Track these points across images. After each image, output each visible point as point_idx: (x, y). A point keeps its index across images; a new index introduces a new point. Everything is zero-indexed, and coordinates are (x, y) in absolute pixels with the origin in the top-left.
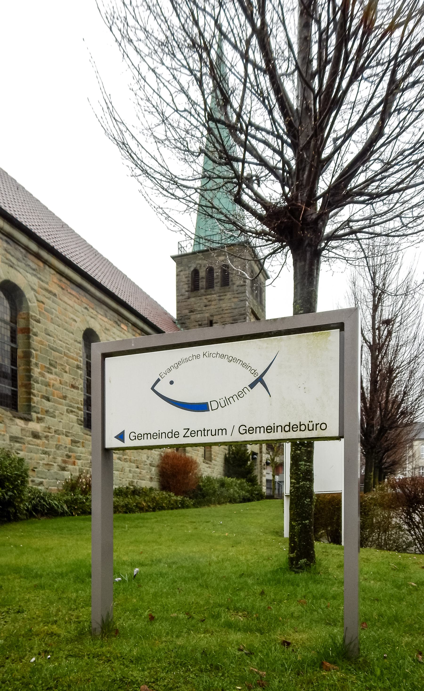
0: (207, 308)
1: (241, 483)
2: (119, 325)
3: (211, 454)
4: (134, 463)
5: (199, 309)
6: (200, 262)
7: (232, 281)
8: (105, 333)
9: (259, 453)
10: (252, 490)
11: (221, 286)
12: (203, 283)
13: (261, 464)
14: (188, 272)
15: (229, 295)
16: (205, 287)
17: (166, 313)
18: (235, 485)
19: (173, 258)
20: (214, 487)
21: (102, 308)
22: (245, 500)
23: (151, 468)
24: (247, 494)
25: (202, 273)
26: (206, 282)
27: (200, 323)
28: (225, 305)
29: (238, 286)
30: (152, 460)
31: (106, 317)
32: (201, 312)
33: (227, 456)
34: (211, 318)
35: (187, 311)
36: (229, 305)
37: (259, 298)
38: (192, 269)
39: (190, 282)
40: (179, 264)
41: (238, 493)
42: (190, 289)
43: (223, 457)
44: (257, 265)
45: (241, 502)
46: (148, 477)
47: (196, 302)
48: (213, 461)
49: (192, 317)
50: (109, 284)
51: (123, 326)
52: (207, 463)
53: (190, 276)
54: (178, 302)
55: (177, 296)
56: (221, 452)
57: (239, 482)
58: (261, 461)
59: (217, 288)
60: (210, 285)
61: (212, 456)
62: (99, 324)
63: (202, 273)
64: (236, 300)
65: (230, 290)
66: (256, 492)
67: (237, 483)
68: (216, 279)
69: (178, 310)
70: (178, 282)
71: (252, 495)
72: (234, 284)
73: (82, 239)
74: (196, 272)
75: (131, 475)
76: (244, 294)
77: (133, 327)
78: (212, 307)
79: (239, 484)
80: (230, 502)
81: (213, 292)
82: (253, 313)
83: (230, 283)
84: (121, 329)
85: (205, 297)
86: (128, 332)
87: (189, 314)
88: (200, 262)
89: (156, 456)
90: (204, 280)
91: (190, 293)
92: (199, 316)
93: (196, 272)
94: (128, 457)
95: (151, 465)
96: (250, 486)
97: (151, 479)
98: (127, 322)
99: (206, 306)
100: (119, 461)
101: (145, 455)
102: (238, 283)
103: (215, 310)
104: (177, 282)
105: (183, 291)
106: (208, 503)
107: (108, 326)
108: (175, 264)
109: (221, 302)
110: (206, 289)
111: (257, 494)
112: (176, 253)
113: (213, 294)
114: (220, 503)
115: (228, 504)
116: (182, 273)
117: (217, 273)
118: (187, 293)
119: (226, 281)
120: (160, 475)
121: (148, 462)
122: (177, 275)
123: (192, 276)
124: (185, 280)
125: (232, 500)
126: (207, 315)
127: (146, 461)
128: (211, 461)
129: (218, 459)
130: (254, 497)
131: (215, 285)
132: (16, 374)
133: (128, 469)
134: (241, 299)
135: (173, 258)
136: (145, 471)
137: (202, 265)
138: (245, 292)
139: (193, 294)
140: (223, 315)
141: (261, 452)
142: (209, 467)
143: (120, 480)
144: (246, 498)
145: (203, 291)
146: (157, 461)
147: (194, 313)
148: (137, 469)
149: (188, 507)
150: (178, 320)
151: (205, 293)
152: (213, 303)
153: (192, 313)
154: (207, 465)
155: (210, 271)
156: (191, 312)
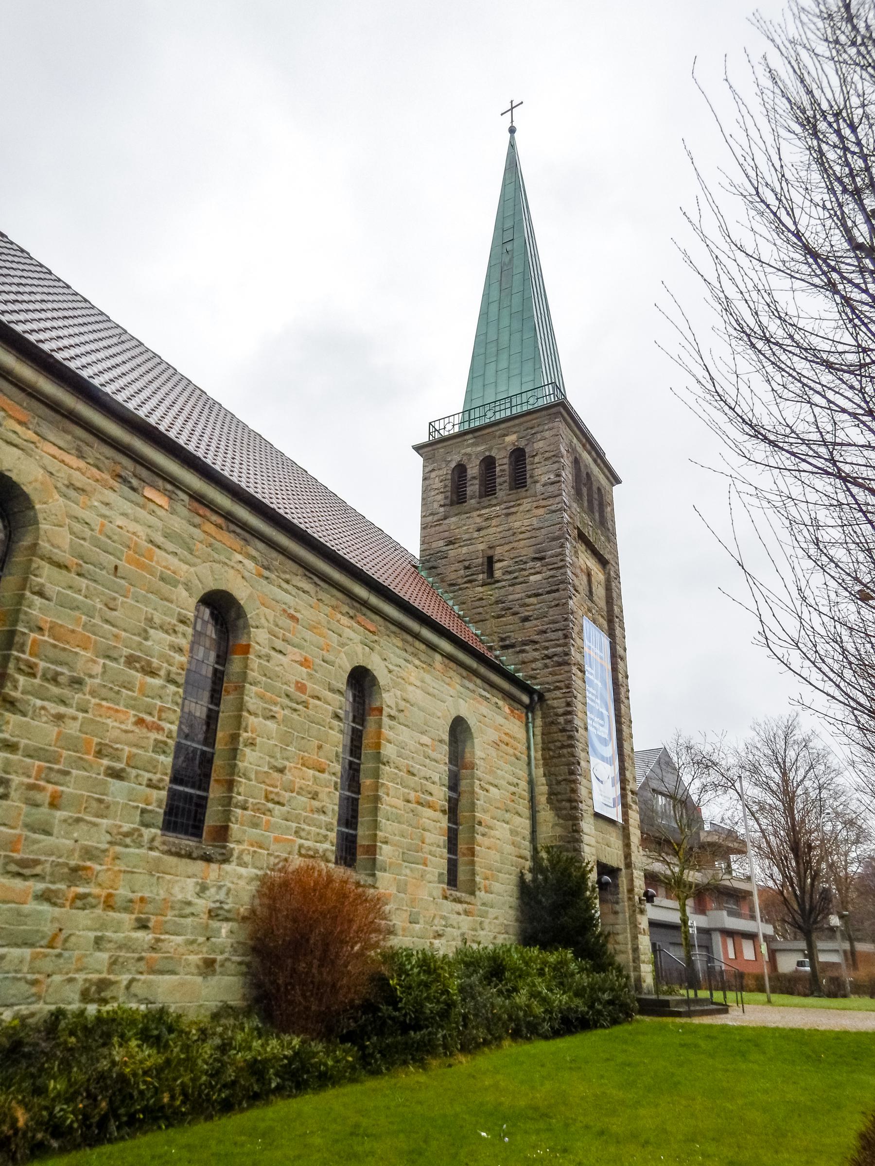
0: (482, 533)
1: (563, 963)
2: (134, 489)
3: (473, 873)
4: (126, 910)
5: (466, 537)
6: (469, 450)
7: (531, 477)
8: (65, 496)
9: (622, 867)
10: (592, 987)
11: (511, 489)
12: (473, 488)
13: (630, 899)
14: (446, 471)
15: (526, 505)
16: (477, 494)
17: (397, 547)
18: (541, 973)
19: (418, 448)
20: (446, 992)
21: (65, 431)
22: (570, 1024)
23: (215, 924)
24: (578, 1001)
25: (473, 470)
26: (480, 485)
27: (467, 563)
28: (517, 523)
29: (544, 486)
30: (222, 896)
31: (81, 456)
32: (470, 541)
33: (528, 877)
34: (490, 553)
35: (441, 543)
36: (526, 522)
37: (597, 515)
38: (453, 465)
39: (448, 489)
40: (427, 459)
41: (544, 1000)
42: (448, 502)
43: (514, 879)
44: (589, 453)
45: (556, 1034)
46: (194, 958)
47: (463, 524)
48: (481, 894)
49: (452, 553)
50: (195, 439)
51: (149, 492)
52: (459, 901)
53: (449, 477)
54: (424, 527)
55: (423, 517)
56: (507, 867)
57: (552, 958)
58: (631, 891)
59: (502, 493)
60: (488, 489)
61: (478, 879)
62: (44, 468)
63: (473, 470)
64: (541, 511)
65: (528, 493)
66: (606, 997)
67: (545, 963)
68: (500, 476)
69: (423, 543)
70: (425, 491)
71: (591, 1007)
72: (537, 482)
73: (148, 350)
74: (461, 469)
75: (104, 956)
76: (558, 499)
77: (196, 505)
78: (492, 530)
79: (555, 968)
80: (516, 1035)
81: (494, 502)
82: (582, 537)
83: (529, 481)
84: (141, 500)
85: (478, 512)
86: (173, 512)
87: (445, 548)
88: (469, 450)
89: (242, 883)
90: (477, 482)
91: (447, 508)
92: (465, 550)
93: (461, 469)
94: (95, 890)
95: (213, 914)
96: (589, 972)
97: (209, 966)
98: (169, 487)
99: (479, 530)
100: (45, 907)
101: (191, 882)
102: (544, 479)
103: (499, 536)
104: (424, 492)
105: (436, 505)
106: (419, 1053)
107: (79, 479)
108: (420, 460)
109: (511, 518)
110: (481, 497)
111: (610, 1002)
112: (424, 438)
113: (495, 505)
114: (470, 1047)
115: (506, 1043)
116: (433, 475)
117: (503, 465)
118: (442, 509)
119: (519, 479)
120: (255, 950)
121: (202, 905)
122: (425, 479)
123: (452, 479)
124: (438, 484)
125: (524, 1029)
126: (481, 547)
127: (189, 904)
128: (473, 893)
129: (496, 886)
130: (599, 1012)
131: (498, 488)
132: (212, 697)
133: (92, 935)
134: (553, 508)
135: (418, 448)
136: (179, 939)
137: (472, 454)
138: (561, 495)
139: (456, 509)
140: (515, 545)
141: (629, 865)
142: (467, 913)
143: (34, 983)
144: (572, 1016)
145: (473, 501)
146: (246, 899)
147: (456, 545)
148: (140, 934)
149: (326, 1079)
150: (422, 562)
151: (477, 506)
152: (494, 522)
153: (451, 547)
154: (459, 907)
155: (489, 463)
156: (451, 543)
